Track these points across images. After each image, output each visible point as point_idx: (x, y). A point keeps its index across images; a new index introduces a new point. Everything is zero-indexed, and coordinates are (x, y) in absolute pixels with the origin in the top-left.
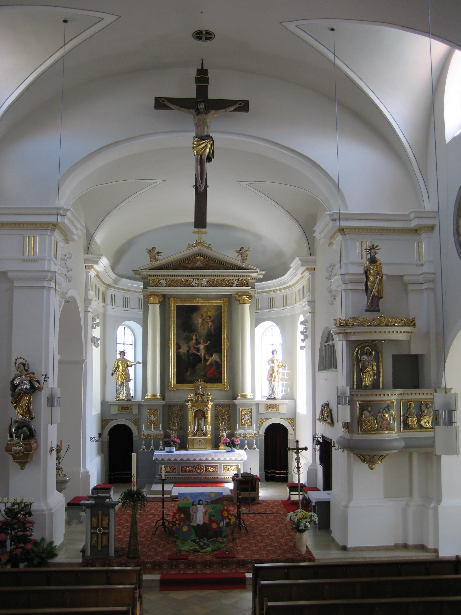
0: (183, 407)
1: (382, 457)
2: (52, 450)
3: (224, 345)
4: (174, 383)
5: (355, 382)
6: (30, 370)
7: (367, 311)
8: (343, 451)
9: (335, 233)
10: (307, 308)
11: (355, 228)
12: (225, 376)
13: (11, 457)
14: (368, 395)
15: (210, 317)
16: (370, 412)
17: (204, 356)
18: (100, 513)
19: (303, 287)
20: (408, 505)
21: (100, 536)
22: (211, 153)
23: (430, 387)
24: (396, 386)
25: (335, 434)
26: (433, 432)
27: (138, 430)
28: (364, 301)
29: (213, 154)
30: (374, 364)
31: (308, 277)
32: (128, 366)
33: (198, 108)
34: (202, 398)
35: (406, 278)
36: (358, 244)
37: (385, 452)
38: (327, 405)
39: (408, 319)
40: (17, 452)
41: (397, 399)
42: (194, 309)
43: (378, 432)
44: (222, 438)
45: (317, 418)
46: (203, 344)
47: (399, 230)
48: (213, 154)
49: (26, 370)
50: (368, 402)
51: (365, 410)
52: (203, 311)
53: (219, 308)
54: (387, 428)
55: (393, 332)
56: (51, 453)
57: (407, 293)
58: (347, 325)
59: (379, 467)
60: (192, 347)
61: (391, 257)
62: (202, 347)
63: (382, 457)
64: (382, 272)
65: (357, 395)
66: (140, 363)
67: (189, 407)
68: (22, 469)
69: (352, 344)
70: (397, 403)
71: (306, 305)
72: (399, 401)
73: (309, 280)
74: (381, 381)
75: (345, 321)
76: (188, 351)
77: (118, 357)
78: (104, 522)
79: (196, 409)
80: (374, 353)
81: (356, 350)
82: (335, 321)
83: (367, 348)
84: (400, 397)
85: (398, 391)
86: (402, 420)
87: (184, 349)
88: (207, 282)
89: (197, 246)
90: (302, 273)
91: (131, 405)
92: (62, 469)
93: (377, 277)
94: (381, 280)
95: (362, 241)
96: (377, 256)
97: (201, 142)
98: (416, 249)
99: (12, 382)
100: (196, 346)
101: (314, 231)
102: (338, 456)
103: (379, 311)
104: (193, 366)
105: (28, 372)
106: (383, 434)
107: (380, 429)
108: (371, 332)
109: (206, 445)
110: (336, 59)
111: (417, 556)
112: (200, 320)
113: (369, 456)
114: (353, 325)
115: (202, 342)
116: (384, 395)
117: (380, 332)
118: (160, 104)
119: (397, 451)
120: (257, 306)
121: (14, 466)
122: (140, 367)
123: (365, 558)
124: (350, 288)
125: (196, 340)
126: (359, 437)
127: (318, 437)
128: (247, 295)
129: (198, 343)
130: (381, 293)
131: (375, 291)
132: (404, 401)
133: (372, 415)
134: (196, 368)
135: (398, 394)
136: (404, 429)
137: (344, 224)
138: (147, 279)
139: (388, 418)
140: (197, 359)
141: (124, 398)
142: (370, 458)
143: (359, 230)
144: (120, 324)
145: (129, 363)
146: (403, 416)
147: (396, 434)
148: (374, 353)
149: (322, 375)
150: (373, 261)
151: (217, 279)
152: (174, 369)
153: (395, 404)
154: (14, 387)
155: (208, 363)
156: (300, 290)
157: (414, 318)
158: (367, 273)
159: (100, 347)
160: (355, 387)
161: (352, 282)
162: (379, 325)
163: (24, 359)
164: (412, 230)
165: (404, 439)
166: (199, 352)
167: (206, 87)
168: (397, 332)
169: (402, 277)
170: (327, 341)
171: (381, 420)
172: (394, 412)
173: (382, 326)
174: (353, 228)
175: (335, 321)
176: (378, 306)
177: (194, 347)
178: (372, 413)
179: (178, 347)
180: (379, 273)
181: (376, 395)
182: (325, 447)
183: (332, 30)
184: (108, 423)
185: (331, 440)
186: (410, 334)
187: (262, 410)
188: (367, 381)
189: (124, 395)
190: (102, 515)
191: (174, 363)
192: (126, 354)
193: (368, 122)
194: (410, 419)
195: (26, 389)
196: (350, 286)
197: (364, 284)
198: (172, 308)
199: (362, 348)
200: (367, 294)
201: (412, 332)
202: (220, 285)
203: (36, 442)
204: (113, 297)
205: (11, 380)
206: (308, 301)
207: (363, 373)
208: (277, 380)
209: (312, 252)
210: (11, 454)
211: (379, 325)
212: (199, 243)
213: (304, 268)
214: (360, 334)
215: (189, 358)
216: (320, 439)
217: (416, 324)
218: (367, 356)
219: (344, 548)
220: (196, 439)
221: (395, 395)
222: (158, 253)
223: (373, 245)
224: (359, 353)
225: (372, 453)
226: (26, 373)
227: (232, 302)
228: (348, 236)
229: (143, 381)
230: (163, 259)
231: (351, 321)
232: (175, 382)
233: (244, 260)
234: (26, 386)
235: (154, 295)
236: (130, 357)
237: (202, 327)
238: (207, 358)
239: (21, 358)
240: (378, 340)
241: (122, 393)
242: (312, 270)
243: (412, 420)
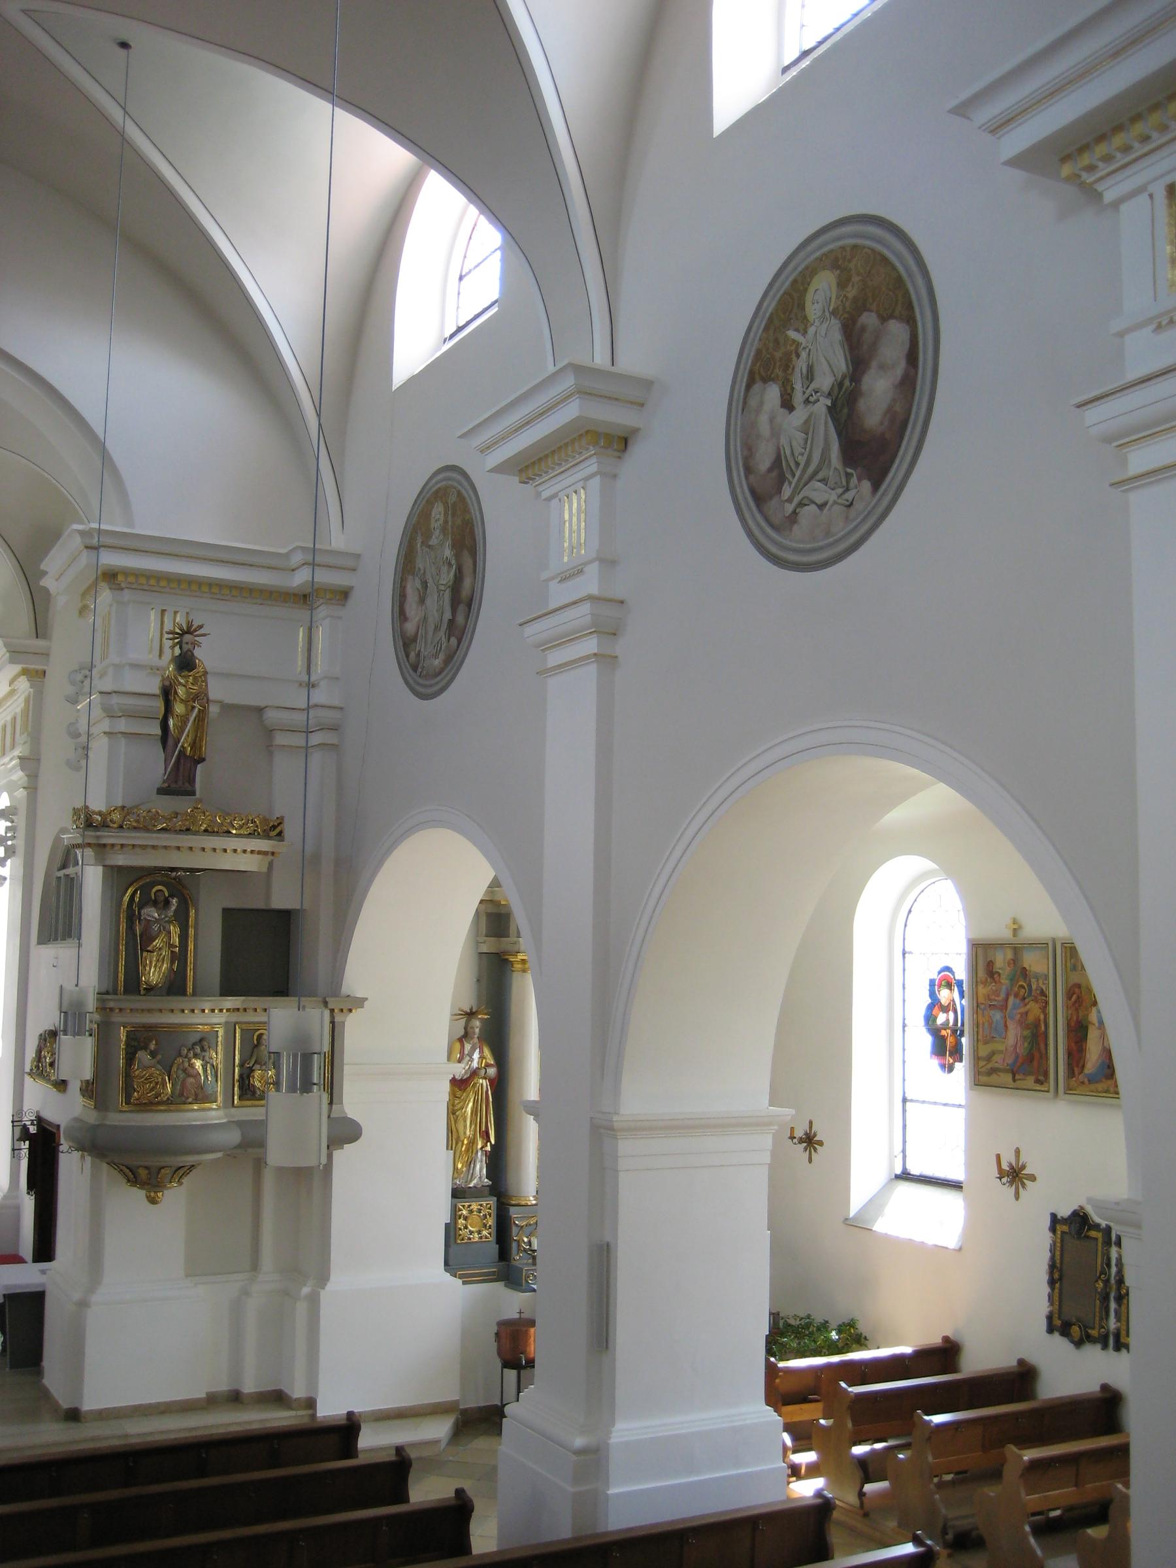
1: (181, 1172)
5: (121, 976)
7: (161, 791)
8: (83, 1157)
9: (95, 583)
10: (19, 776)
11: (149, 575)
14: (150, 1011)
16: (153, 1054)
19: (15, 718)
20: (246, 1292)
23: (312, 994)
24: (227, 990)
25: (66, 1110)
26: (263, 1110)
28: (156, 767)
30: (175, 930)
31: (26, 693)
35: (271, 716)
36: (152, 617)
37: (190, 1159)
39: (265, 820)
41: (227, 1023)
43: (173, 1107)
45: (27, 1069)
47: (261, 591)
50: (151, 1030)
51: (141, 1049)
54: (196, 1095)
55: (225, 851)
57: (271, 754)
58: (104, 825)
59: (175, 1197)
61: (235, 656)
63: (181, 1172)
64: (206, 695)
65: (121, 1010)
69: (118, 877)
70: (226, 1032)
71: (14, 767)
72: (231, 1028)
73: (27, 701)
74: (190, 974)
75: (100, 813)
81: (130, 892)
82: (76, 812)
83: (160, 887)
84: (234, 1018)
85: (231, 1002)
86: (237, 1077)
90: (11, 683)
93: (193, 707)
94: (203, 714)
95: (163, 611)
96: (197, 652)
98: (301, 645)
101: (45, 573)
102: (72, 1168)
103: (193, 793)
106: (188, 1111)
107: (179, 1100)
108: (165, 847)
110: (129, 122)
111: (262, 1421)
113: (146, 1168)
114: (121, 827)
116: (193, 1011)
117: (191, 848)
119: (219, 1155)
123: (126, 1436)
124: (123, 729)
126: (124, 1118)
127: (28, 1119)
130: (201, 747)
131: (185, 741)
132: (244, 1027)
133: (158, 1062)
135: (228, 1010)
136: (240, 1098)
137: (111, 559)
139: (201, 1071)
142: (150, 1173)
143: (200, 588)
146: (242, 1065)
147: (221, 1113)
148: (174, 901)
149: (45, 955)
150: (185, 663)
153: (220, 1034)
157: (282, 818)
158: (167, 693)
160: (121, 988)
161: (131, 715)
162: (188, 830)
165: (240, 1124)
168: (235, 851)
169: (260, 710)
170: (64, 866)
171: (182, 1076)
172: (218, 1056)
173: (196, 833)
174: (235, 587)
175: (76, 812)
176: (191, 780)
178: (159, 1057)
180: (199, 697)
181: (172, 1011)
183: (124, 45)
185: (58, 1126)
186: (270, 857)
188: (154, 973)
193: (207, 308)
194: (257, 1073)
196: (122, 725)
197: (158, 722)
199: (145, 889)
200: (164, 748)
201: (273, 854)
206: (20, 758)
207: (145, 954)
209: (40, 629)
211: (188, 830)
213: (17, 668)
214: (138, 850)
216: (32, 1124)
217: (286, 834)
218: (158, 909)
219: (73, 1415)
221: (221, 1010)
223: (190, 625)
224: (137, 900)
225: (154, 1162)
228: (127, 595)
231: (116, 816)
240: (185, 870)
242: (37, 676)
243: (262, 1077)
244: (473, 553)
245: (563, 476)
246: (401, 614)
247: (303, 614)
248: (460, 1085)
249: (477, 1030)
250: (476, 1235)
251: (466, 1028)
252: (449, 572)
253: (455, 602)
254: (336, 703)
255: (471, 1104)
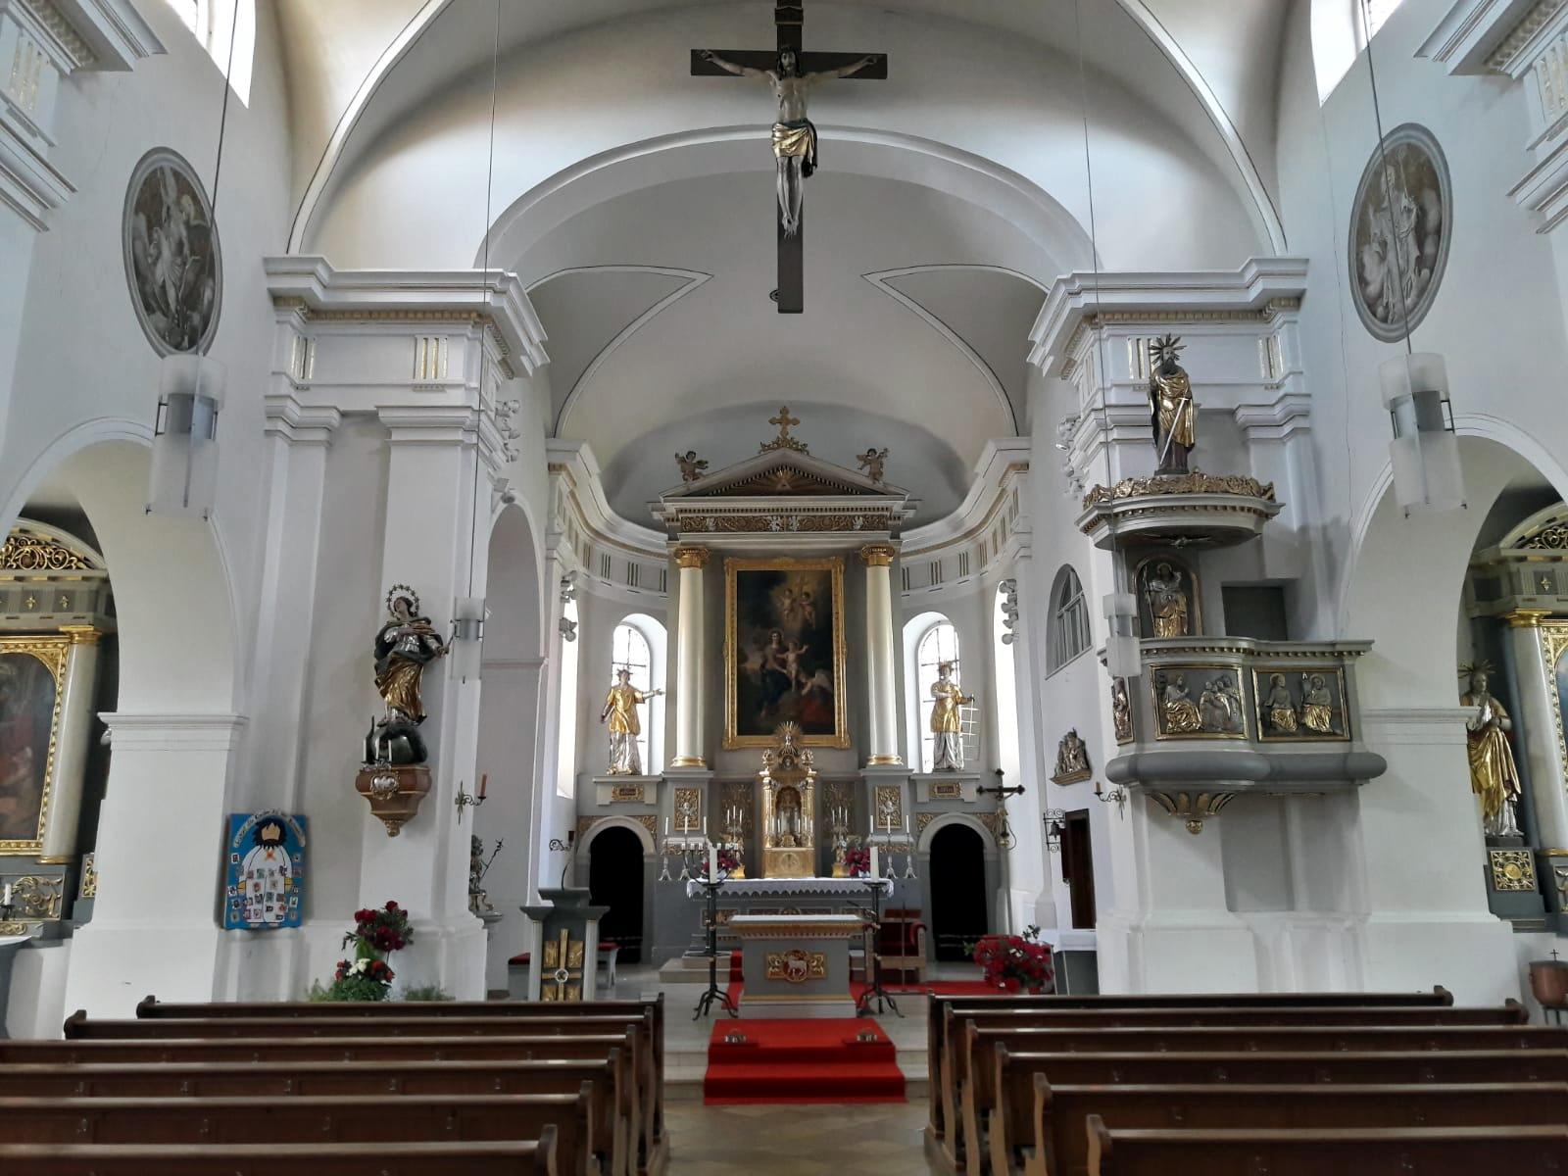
0: (752, 785)
2: (461, 801)
3: (838, 653)
4: (733, 734)
6: (421, 615)
12: (841, 720)
13: (368, 803)
15: (807, 594)
16: (1181, 688)
17: (796, 677)
18: (564, 933)
21: (561, 987)
22: (811, 153)
27: (655, 840)
29: (815, 158)
32: (635, 701)
33: (781, 64)
34: (792, 762)
36: (1130, 348)
38: (1074, 735)
40: (383, 792)
42: (773, 579)
44: (838, 852)
46: (793, 652)
48: (815, 158)
49: (411, 614)
52: (794, 584)
53: (826, 579)
56: (460, 809)
60: (770, 658)
62: (791, 657)
66: (661, 694)
67: (766, 780)
68: (392, 835)
76: (763, 666)
77: (615, 681)
78: (572, 956)
79: (779, 786)
80: (1178, 575)
87: (754, 663)
88: (801, 522)
89: (777, 448)
91: (641, 784)
92: (484, 891)
95: (1138, 340)
97: (790, 133)
99: (380, 639)
100: (779, 656)
104: (774, 700)
105: (416, 618)
109: (804, 867)
112: (787, 602)
115: (791, 646)
118: (703, 64)
120: (902, 580)
121: (373, 825)
122: (660, 702)
125: (780, 642)
128: (883, 548)
129: (783, 649)
134: (780, 702)
136: (1264, 734)
138: (678, 520)
140: (782, 683)
141: (627, 768)
144: (617, 622)
145: (638, 695)
146: (1261, 705)
151: (821, 517)
152: (733, 703)
154: (383, 647)
155: (805, 691)
156: (995, 534)
157: (1271, 484)
159: (577, 640)
163: (408, 589)
164: (1252, 311)
166: (785, 668)
167: (800, 27)
169: (1232, 413)
177: (775, 659)
179: (742, 658)
182: (1074, 839)
184: (590, 825)
187: (923, 795)
189: (627, 763)
190: (570, 937)
191: (733, 691)
192: (631, 677)
195: (410, 651)
198: (728, 579)
202: (829, 529)
203: (427, 772)
204: (607, 561)
205: (378, 632)
207: (1157, 620)
208: (952, 727)
210: (368, 797)
212: (779, 444)
215: (764, 681)
216: (1061, 822)
220: (783, 852)
222: (700, 462)
226: (411, 619)
227: (855, 562)
228: (1106, 331)
229: (664, 737)
230: (711, 476)
232: (736, 734)
233: (876, 475)
234: (411, 644)
235: (692, 548)
236: (639, 681)
237: (792, 614)
238: (804, 680)
239: (401, 587)
241: (622, 757)
244: (1435, 186)
245: (1538, 40)
246: (1360, 279)
247: (1257, 327)
248: (1477, 735)
249: (1484, 684)
250: (1516, 883)
251: (1471, 683)
252: (1409, 217)
253: (1420, 234)
254: (1304, 391)
255: (1489, 754)
